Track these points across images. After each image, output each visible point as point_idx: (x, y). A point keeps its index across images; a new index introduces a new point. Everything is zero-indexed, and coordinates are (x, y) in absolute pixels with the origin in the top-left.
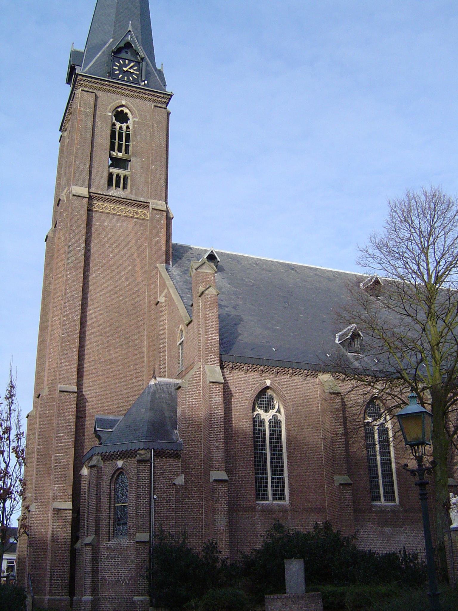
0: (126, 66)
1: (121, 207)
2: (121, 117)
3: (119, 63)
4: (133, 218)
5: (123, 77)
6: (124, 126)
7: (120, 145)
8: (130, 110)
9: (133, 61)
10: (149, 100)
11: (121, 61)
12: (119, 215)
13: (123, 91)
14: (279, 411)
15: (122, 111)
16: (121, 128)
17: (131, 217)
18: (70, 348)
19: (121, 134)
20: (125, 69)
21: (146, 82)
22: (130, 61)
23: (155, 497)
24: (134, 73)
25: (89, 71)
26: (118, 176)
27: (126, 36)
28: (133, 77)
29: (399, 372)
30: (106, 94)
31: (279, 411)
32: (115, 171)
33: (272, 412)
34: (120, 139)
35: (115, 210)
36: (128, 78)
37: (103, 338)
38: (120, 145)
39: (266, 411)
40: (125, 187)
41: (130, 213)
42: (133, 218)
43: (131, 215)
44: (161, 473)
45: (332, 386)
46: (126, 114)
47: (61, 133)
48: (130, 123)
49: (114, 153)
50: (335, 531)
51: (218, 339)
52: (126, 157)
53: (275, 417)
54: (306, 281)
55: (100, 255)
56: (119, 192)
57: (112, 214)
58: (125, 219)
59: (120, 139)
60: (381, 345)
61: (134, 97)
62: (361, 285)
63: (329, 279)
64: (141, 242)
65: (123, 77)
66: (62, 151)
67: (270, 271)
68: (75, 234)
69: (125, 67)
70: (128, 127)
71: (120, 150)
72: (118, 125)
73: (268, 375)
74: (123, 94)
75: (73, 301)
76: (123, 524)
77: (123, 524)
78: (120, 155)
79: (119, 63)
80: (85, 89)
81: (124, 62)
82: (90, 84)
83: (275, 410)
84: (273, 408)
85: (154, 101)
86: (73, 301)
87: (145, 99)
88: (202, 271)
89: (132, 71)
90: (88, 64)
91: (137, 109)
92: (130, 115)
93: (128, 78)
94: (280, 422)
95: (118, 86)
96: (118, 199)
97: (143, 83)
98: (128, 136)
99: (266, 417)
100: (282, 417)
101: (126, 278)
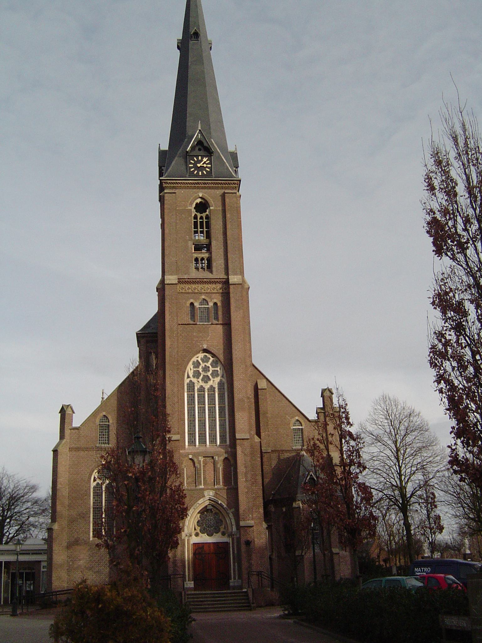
0: (199, 162)
3: (194, 160)
5: (198, 173)
6: (204, 215)
11: (195, 158)
16: (201, 218)
20: (199, 165)
22: (203, 157)
24: (207, 167)
28: (206, 171)
29: (467, 514)
45: (411, 418)
50: (310, 406)
60: (458, 514)
65: (198, 173)
66: (250, 356)
69: (199, 163)
72: (199, 215)
79: (194, 160)
81: (198, 158)
89: (205, 165)
91: (213, 196)
93: (202, 173)
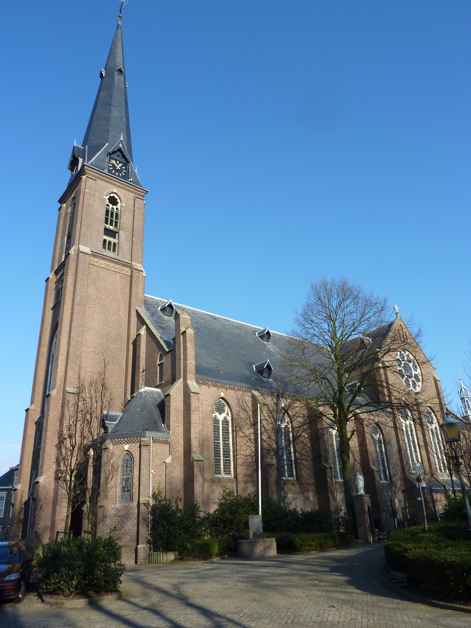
1: (112, 264)
2: (113, 201)
4: (120, 273)
6: (115, 207)
7: (112, 221)
8: (119, 197)
9: (122, 163)
10: (132, 192)
12: (110, 270)
13: (115, 183)
14: (227, 414)
15: (114, 197)
17: (118, 272)
18: (74, 361)
19: (112, 213)
21: (131, 179)
23: (153, 471)
25: (92, 164)
26: (110, 242)
27: (119, 143)
30: (104, 182)
31: (227, 414)
32: (108, 239)
33: (224, 415)
34: (112, 216)
35: (107, 266)
36: (119, 174)
37: (97, 356)
38: (112, 221)
39: (220, 414)
40: (114, 251)
41: (118, 269)
42: (120, 273)
43: (118, 271)
44: (156, 455)
46: (116, 199)
47: (59, 205)
48: (119, 206)
49: (107, 226)
51: (194, 363)
52: (115, 230)
53: (225, 418)
54: (225, 328)
55: (96, 296)
56: (110, 254)
57: (105, 269)
58: (114, 273)
59: (112, 216)
61: (122, 188)
62: (256, 333)
63: (237, 327)
64: (125, 291)
67: (203, 319)
68: (81, 280)
70: (117, 209)
71: (111, 224)
72: (111, 206)
73: (222, 389)
74: (115, 185)
75: (78, 328)
76: (127, 491)
77: (127, 491)
78: (111, 228)
80: (89, 176)
82: (93, 173)
83: (226, 413)
84: (224, 412)
85: (135, 193)
86: (78, 328)
87: (130, 191)
88: (183, 316)
90: (92, 158)
92: (119, 200)
94: (228, 422)
95: (112, 178)
96: (109, 258)
97: (129, 180)
98: (117, 214)
99: (221, 417)
100: (229, 419)
101: (114, 315)
